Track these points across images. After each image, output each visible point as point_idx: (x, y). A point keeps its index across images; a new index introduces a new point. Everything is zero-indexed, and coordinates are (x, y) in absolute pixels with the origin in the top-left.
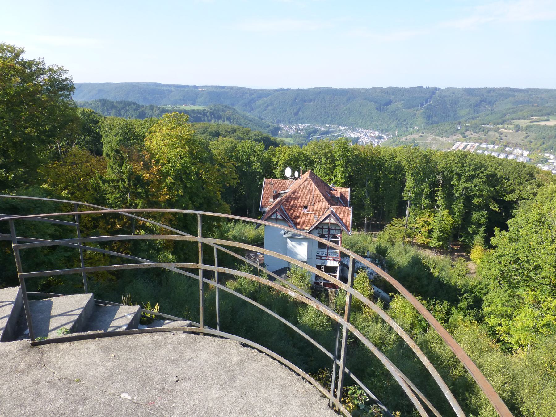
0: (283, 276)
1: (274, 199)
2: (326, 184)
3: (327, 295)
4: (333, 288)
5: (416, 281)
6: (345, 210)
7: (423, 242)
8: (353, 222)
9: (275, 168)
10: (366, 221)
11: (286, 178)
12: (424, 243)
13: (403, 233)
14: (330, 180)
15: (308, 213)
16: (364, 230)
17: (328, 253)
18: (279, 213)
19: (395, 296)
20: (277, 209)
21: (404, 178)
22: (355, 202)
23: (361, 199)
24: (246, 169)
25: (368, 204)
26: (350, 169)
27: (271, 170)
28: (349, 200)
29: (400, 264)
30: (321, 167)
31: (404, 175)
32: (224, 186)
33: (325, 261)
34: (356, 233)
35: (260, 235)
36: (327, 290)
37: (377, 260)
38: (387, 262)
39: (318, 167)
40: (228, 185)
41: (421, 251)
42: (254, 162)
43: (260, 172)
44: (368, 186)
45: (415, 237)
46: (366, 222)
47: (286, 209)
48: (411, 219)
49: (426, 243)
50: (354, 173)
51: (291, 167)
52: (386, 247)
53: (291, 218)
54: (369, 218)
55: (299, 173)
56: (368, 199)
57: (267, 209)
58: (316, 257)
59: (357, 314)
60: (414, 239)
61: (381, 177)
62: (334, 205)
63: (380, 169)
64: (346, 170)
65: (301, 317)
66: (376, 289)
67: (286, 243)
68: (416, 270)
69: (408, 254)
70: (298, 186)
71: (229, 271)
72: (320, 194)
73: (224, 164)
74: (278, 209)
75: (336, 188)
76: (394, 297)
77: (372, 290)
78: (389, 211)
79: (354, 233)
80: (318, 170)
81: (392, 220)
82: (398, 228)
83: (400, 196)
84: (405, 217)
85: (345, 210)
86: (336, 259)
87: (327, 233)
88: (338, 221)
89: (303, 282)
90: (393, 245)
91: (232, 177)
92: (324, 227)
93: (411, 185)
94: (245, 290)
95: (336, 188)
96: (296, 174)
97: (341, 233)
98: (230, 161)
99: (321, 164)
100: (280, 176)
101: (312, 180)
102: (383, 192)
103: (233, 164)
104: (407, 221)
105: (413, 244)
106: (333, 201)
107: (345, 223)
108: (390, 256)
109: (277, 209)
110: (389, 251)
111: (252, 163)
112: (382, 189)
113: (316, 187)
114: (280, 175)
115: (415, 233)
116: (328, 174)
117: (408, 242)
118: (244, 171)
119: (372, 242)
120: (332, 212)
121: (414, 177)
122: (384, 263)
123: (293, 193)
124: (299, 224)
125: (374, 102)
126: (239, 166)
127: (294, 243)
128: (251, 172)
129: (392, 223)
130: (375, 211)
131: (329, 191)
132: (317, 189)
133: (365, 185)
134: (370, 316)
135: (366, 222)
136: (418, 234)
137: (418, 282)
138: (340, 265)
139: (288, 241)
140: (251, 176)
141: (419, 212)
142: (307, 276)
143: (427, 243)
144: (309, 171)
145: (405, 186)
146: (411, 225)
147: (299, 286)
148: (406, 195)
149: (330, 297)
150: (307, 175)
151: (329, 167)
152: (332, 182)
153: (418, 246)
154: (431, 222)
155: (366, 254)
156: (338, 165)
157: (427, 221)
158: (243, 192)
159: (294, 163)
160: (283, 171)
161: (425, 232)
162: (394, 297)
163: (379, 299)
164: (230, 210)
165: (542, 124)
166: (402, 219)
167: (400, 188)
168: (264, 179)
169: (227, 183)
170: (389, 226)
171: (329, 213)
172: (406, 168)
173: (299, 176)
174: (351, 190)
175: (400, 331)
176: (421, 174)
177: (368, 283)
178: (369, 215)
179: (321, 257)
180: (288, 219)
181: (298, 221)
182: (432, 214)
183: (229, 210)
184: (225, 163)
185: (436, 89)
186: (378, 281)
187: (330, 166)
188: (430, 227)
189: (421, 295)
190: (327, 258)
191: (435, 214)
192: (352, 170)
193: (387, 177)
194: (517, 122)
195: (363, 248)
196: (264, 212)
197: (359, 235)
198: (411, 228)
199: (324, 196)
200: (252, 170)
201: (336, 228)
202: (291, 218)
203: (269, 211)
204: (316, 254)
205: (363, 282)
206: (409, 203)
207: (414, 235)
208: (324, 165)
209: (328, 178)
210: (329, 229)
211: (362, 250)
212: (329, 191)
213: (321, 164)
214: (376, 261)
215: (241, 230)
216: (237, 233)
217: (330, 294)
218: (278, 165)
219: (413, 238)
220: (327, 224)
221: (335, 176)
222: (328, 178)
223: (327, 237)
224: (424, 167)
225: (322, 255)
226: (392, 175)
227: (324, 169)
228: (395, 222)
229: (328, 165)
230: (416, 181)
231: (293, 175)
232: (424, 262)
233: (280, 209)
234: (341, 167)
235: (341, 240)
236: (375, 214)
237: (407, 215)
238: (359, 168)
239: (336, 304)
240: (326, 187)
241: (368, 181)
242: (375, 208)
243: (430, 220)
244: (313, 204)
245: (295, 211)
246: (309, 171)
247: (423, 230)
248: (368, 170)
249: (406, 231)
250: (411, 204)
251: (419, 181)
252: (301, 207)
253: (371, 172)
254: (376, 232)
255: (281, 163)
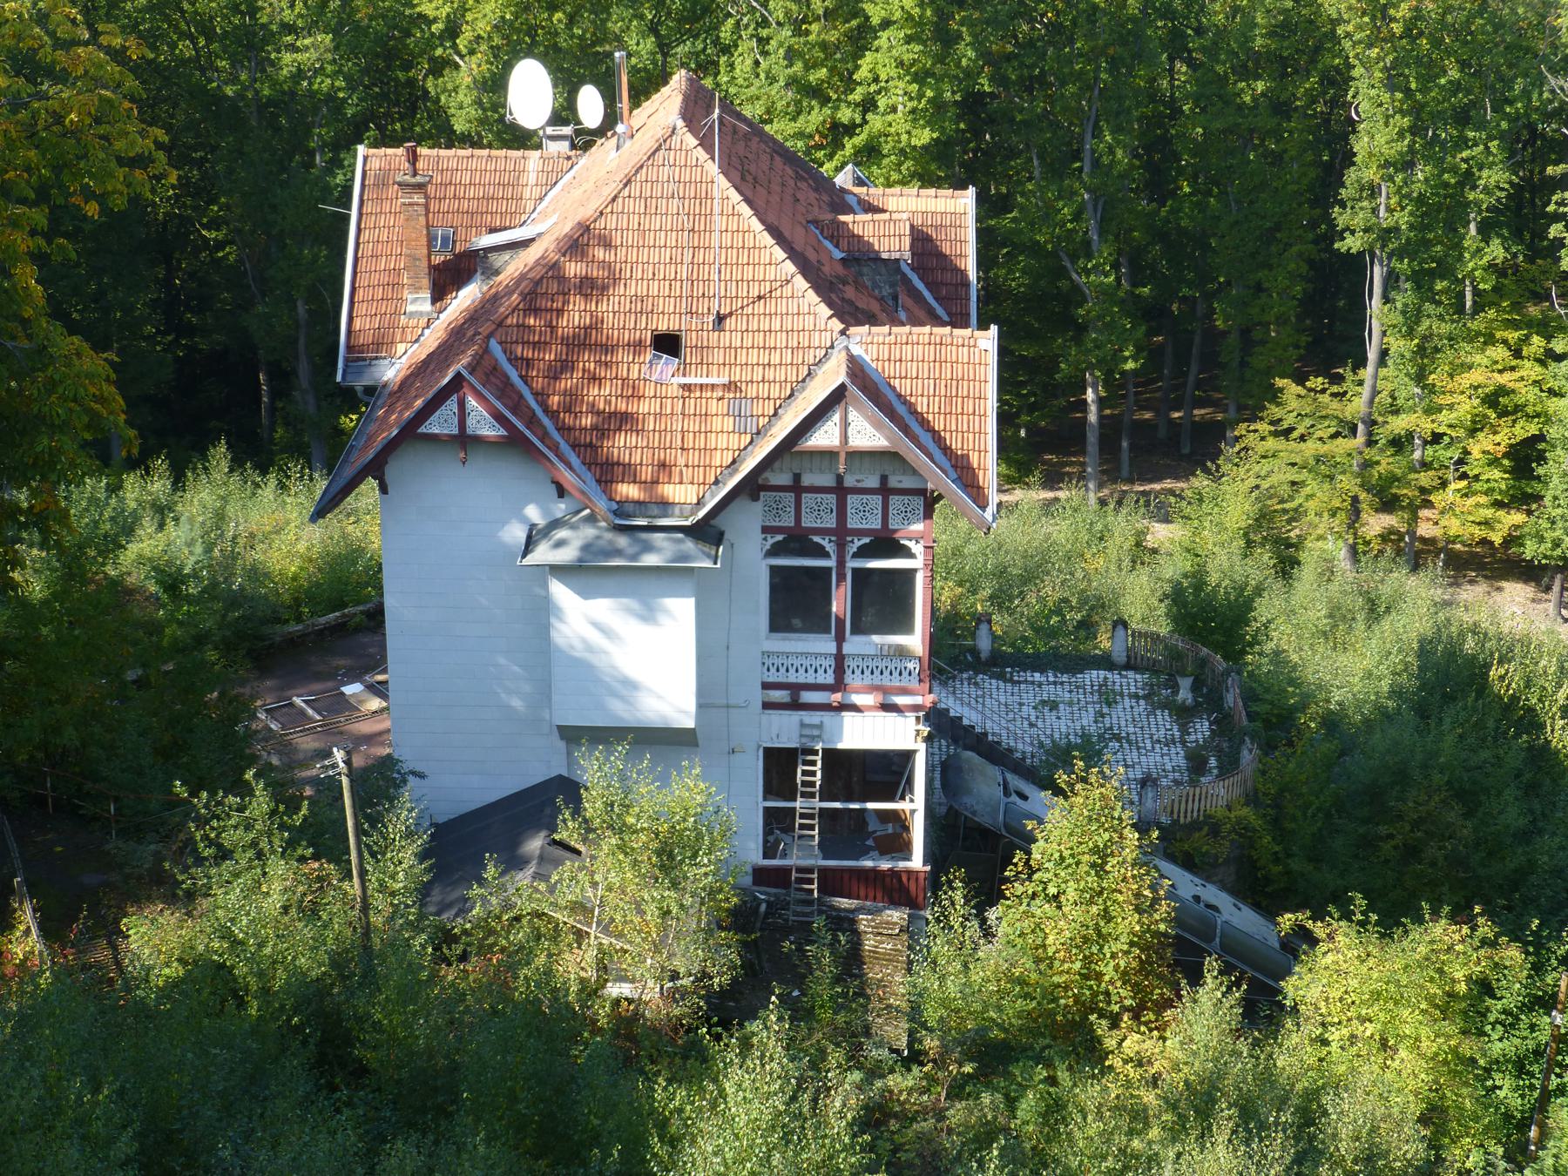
0: (535, 844)
1: (440, 293)
2: (803, 170)
3: (852, 961)
4: (895, 903)
5: (1452, 816)
6: (950, 353)
7: (1479, 533)
8: (1005, 419)
9: (439, 67)
10: (1093, 408)
11: (521, 139)
12: (1484, 542)
13: (1348, 483)
14: (837, 132)
15: (687, 387)
16: (1082, 477)
17: (840, 658)
18: (479, 396)
19: (1319, 930)
20: (460, 365)
21: (1339, 103)
22: (1017, 281)
23: (1054, 254)
24: (234, 80)
25: (1106, 293)
26: (967, 54)
27: (411, 83)
28: (972, 275)
29: (1337, 696)
30: (763, 41)
31: (1338, 80)
32: (63, 221)
33: (826, 718)
34: (1031, 496)
35: (361, 551)
36: (844, 923)
37: (1185, 684)
38: (1249, 697)
39: (747, 45)
40: (92, 209)
41: (1473, 593)
42: (289, 28)
43: (330, 98)
44: (1096, 163)
45: (1428, 504)
46: (1093, 417)
47: (529, 363)
48: (1397, 380)
49: (1497, 539)
50: (999, 79)
51: (552, 58)
52: (1241, 589)
53: (563, 429)
54: (1115, 389)
55: (610, 98)
56: (1104, 253)
57: (391, 372)
58: (758, 696)
59: (1063, 1075)
60: (1424, 513)
61: (1187, 97)
62: (873, 320)
63: (1176, 45)
64: (940, 58)
65: (673, 1142)
66: (1188, 884)
67: (544, 611)
68: (1450, 739)
69: (1386, 624)
70: (608, 191)
72: (768, 240)
73: (47, 54)
74: (472, 369)
75: (874, 194)
76: (1314, 941)
77: (1164, 907)
78: (1245, 332)
79: (1018, 494)
80: (743, 65)
81: (1274, 395)
82: (1311, 447)
83: (1314, 225)
84: (1354, 370)
85: (950, 353)
86: (901, 700)
87: (831, 522)
88: (906, 430)
89: (674, 885)
90: (1287, 565)
91: (120, 145)
92: (807, 480)
93: (1391, 152)
94: (261, 975)
95: (874, 194)
97: (928, 514)
98: (95, 35)
99: (765, 23)
100: (482, 122)
101: (705, 143)
102: (1202, 207)
103: (118, 55)
104: (1375, 392)
105: (1417, 554)
106: (858, 285)
107: (955, 443)
108: (1269, 647)
109: (460, 365)
110: (1264, 610)
111: (270, 38)
112: (1193, 181)
113: (735, 197)
114: (474, 112)
115: (1425, 478)
116: (817, 93)
117: (1384, 537)
118: (219, 97)
119: (1141, 553)
120: (857, 369)
121: (1408, 92)
122: (1232, 698)
123: (579, 242)
124: (628, 472)
125: (414, 165)
126: (184, 62)
127: (603, 608)
128: (271, 102)
129: (1274, 411)
130: (1151, 333)
131: (827, 217)
132: (746, 210)
133: (1077, 156)
134: (1155, 1081)
135: (1093, 417)
136: (1444, 484)
137: (1467, 815)
138: (929, 739)
139: (559, 590)
140: (278, 129)
141: (1445, 328)
142: (699, 837)
143: (1510, 541)
144: (679, 79)
145: (1348, 158)
146: (1399, 424)
147: (652, 911)
148: (1359, 221)
149: (874, 973)
150: (666, 105)
151: (824, 46)
152: (850, 145)
153: (1447, 565)
154: (1527, 394)
155: (1104, 642)
156: (886, 24)
157: (1502, 391)
158: (220, 245)
159: (572, 20)
160: (495, 85)
161: (1494, 462)
162: (1314, 941)
163: (1211, 965)
164: (121, 385)
166: (1338, 379)
167: (1313, 173)
168: (361, 150)
169: (88, 195)
170: (1255, 435)
171: (833, 375)
172: (1353, 28)
173: (611, 118)
174: (981, 199)
176: (1454, 74)
177: (1129, 854)
178: (1109, 367)
179: (796, 688)
180: (544, 436)
181: (622, 445)
182: (1536, 339)
183: (110, 390)
184: (59, 44)
186: (1195, 826)
187: (833, 36)
188: (1524, 429)
189: (1490, 913)
190: (836, 697)
191: (1549, 338)
192: (986, 56)
193: (1229, 100)
195: (1083, 601)
196: (371, 390)
197: (1048, 507)
198: (1399, 444)
199: (794, 255)
200: (274, 83)
201: (893, 482)
202: (563, 429)
203: (406, 384)
204: (758, 676)
205: (1095, 850)
206: (1378, 273)
207: (1423, 490)
208: (786, 32)
209: (815, 118)
210: (841, 491)
211: (1074, 617)
212: (827, 217)
213: (765, 23)
214: (1175, 689)
215: (220, 517)
216: (190, 544)
217: (869, 944)
218: (462, 43)
219: (1413, 510)
220: (829, 455)
221: (868, 105)
222: (815, 118)
223: (830, 547)
224: (1468, 22)
225: (802, 678)
226: (1260, 86)
227: (791, 55)
228: (1294, 404)
229: (815, 27)
230: (1420, 119)
231: (564, 114)
232: (1504, 679)
233: (486, 369)
234: (909, 40)
235: (931, 567)
236: (1153, 356)
237: (1372, 355)
238: (1031, 43)
239: (915, 1013)
240: (807, 194)
241: (1097, 134)
242: (1152, 314)
243: (1524, 379)
244: (720, 319)
245: (594, 379)
246: (679, 79)
247: (1476, 451)
248: (1092, 56)
249: (1367, 465)
250: (1391, 280)
251: (1437, 117)
252: (637, 346)
253: (1114, 64)
254: (1168, 484)
255: (483, 27)
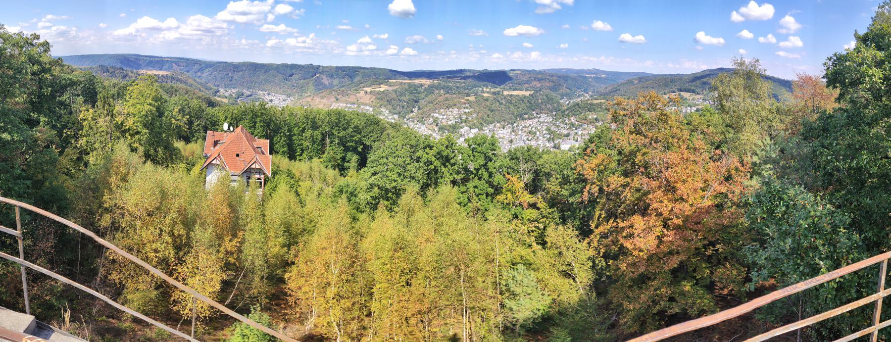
71: (858, 303)
96: (232, 128)
165: (378, 89)
175: (789, 290)
185: (320, 66)
194: (365, 89)
231: (229, 129)
